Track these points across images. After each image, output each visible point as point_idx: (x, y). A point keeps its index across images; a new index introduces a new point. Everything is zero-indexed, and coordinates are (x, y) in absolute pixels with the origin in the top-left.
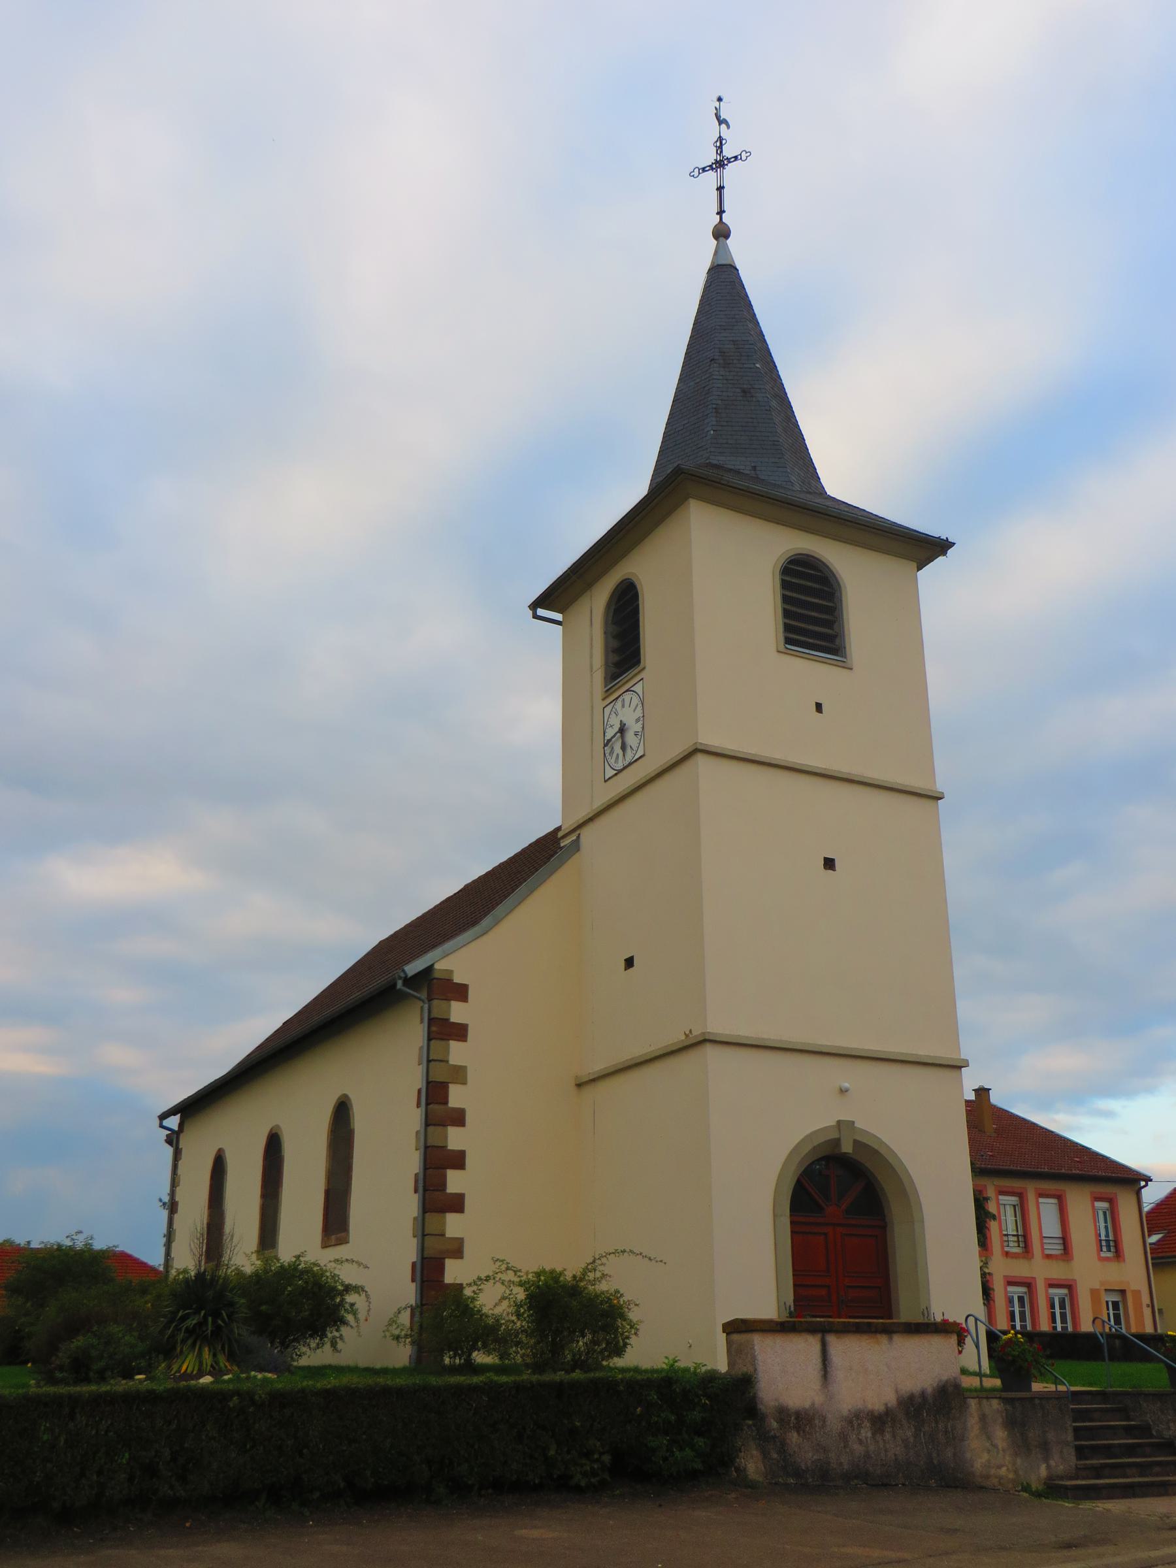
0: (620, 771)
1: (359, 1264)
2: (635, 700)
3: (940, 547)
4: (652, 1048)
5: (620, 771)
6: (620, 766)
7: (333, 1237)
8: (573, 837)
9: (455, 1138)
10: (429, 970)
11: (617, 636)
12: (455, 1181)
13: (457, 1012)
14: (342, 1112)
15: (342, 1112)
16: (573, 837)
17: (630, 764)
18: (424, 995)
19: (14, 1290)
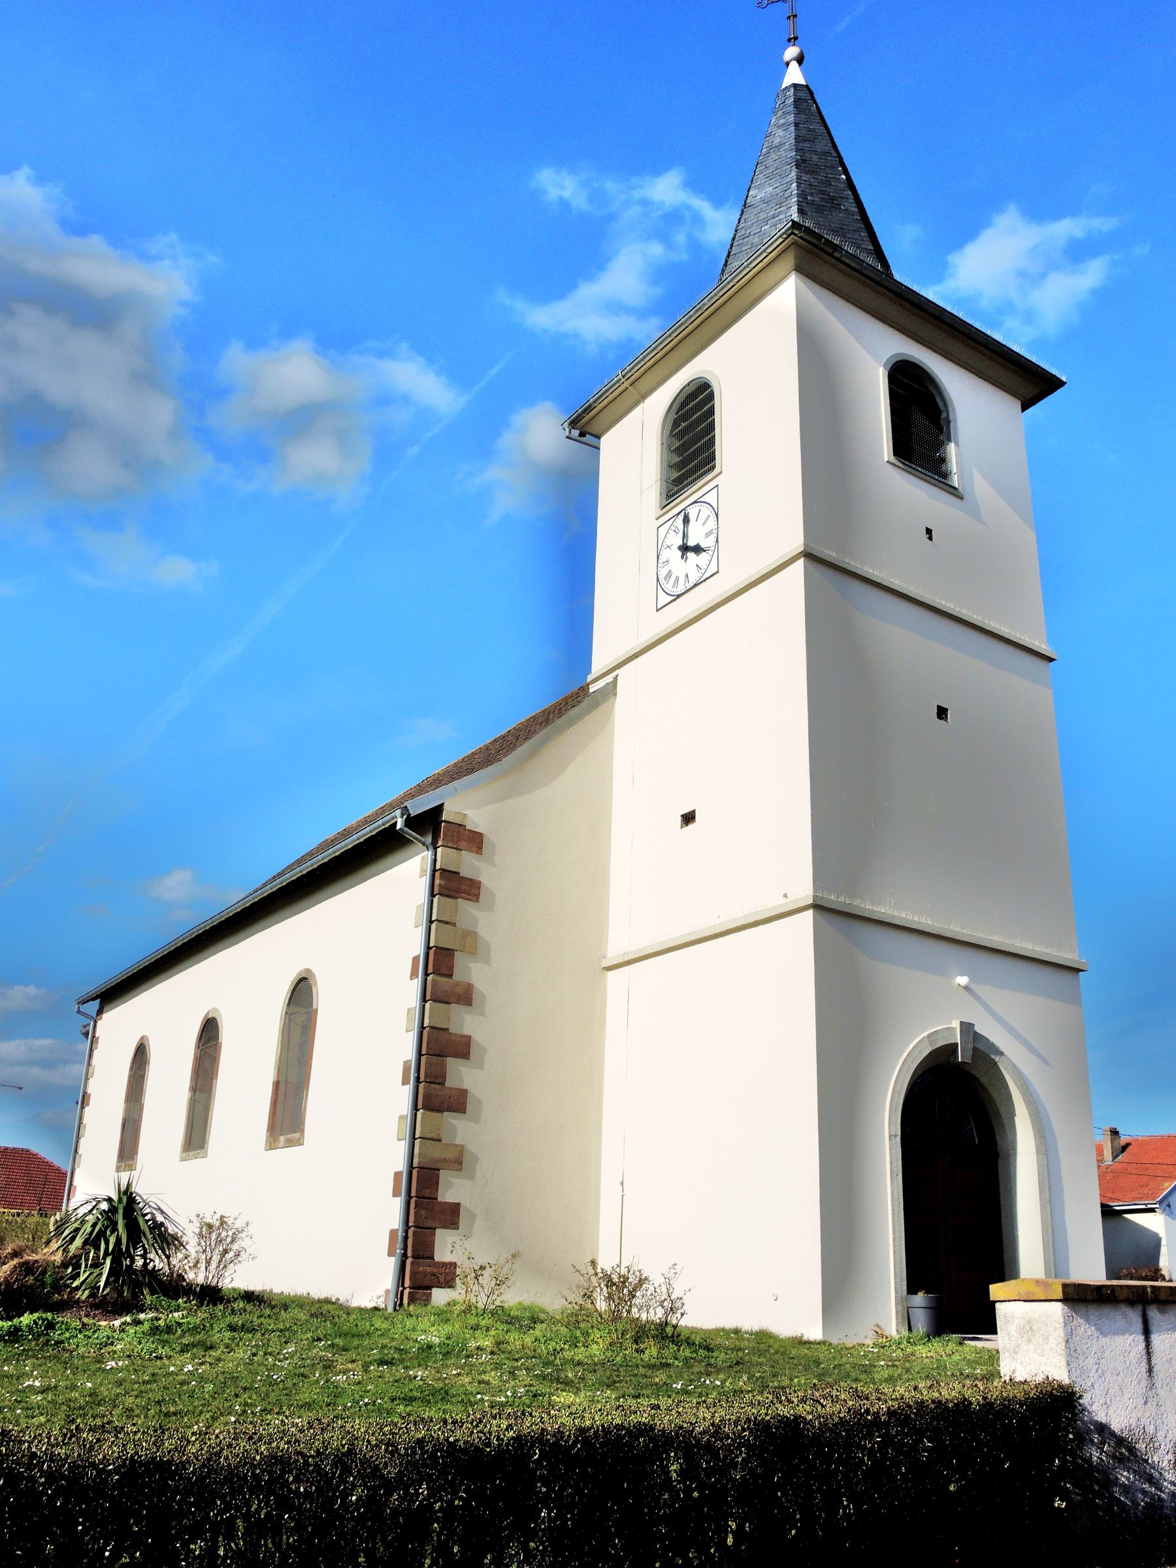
0: (679, 596)
1: (1150, 1370)
2: (706, 511)
3: (1023, 410)
4: (719, 921)
5: (679, 596)
6: (681, 588)
7: (282, 1138)
8: (609, 679)
9: (465, 1022)
10: (439, 809)
11: (679, 451)
12: (460, 1074)
13: (467, 864)
14: (301, 991)
15: (301, 991)
16: (609, 679)
17: (695, 585)
18: (429, 839)
19: (403, 1084)
